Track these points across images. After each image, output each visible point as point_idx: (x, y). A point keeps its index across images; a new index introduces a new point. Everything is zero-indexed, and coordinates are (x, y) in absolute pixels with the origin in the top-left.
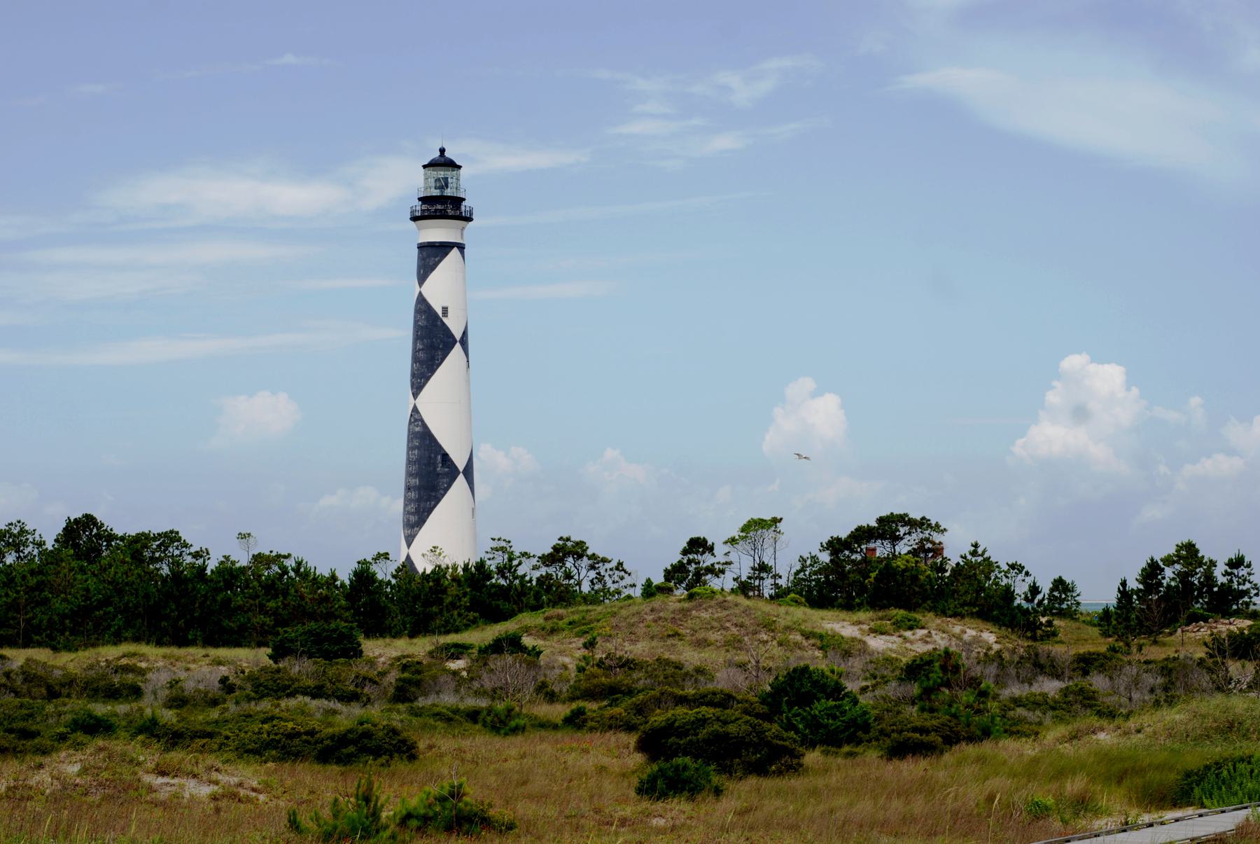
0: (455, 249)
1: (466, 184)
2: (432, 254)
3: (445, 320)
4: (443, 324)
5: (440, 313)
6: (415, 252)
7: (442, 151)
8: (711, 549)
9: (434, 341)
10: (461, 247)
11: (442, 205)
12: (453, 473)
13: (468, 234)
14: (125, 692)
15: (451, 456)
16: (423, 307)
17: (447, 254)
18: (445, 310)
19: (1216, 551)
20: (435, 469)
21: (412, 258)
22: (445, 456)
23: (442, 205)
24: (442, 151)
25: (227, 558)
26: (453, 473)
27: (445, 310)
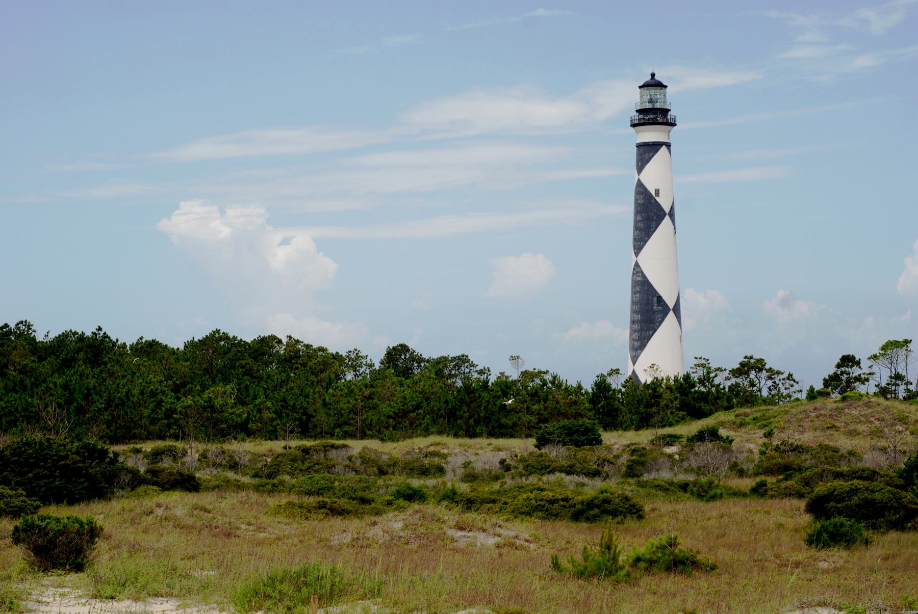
0: (664, 148)
1: (672, 99)
2: (647, 151)
3: (657, 199)
4: (656, 202)
7: (653, 75)
8: (858, 363)
9: (649, 214)
10: (668, 145)
11: (654, 115)
12: (665, 310)
13: (674, 135)
17: (658, 151)
18: (657, 192)
20: (652, 307)
22: (660, 298)
23: (654, 115)
24: (653, 75)
26: (665, 310)
27: (657, 192)
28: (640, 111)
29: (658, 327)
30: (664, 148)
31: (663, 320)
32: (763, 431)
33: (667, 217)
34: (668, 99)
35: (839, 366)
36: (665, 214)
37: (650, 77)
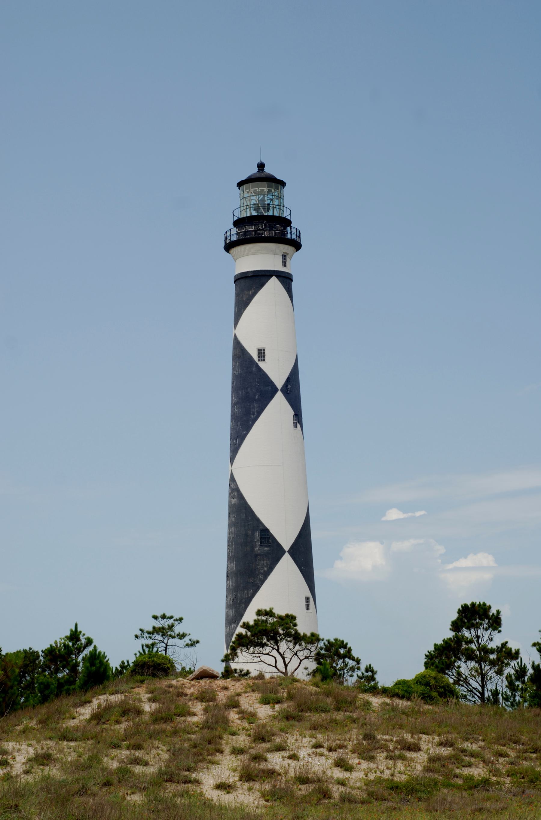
0: (274, 282)
1: (293, 205)
2: (250, 284)
3: (261, 364)
4: (260, 369)
5: (255, 356)
6: (232, 286)
7: (261, 166)
8: (495, 622)
9: (251, 390)
10: (286, 279)
11: (265, 227)
12: (275, 552)
13: (297, 264)
14: (261, 774)
15: (272, 531)
16: (240, 352)
17: (262, 285)
18: (262, 353)
19: (361, 661)
20: (253, 548)
21: (229, 292)
22: (265, 532)
23: (265, 227)
24: (261, 166)
25: (499, 632)
26: (275, 552)
27: (262, 353)
28: (238, 223)
29: (263, 582)
30: (274, 282)
31: (271, 569)
32: (150, 696)
33: (279, 397)
34: (287, 202)
35: (456, 626)
36: (275, 390)
37: (256, 170)
